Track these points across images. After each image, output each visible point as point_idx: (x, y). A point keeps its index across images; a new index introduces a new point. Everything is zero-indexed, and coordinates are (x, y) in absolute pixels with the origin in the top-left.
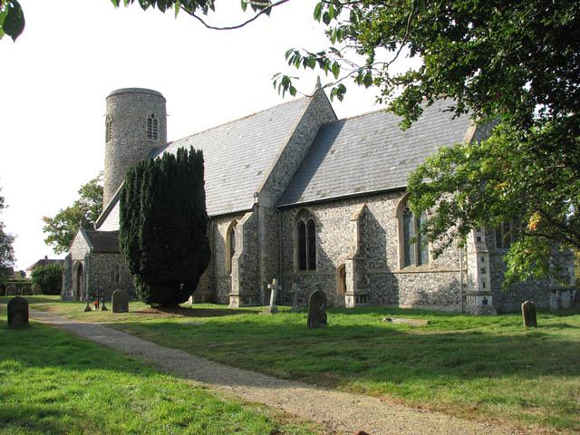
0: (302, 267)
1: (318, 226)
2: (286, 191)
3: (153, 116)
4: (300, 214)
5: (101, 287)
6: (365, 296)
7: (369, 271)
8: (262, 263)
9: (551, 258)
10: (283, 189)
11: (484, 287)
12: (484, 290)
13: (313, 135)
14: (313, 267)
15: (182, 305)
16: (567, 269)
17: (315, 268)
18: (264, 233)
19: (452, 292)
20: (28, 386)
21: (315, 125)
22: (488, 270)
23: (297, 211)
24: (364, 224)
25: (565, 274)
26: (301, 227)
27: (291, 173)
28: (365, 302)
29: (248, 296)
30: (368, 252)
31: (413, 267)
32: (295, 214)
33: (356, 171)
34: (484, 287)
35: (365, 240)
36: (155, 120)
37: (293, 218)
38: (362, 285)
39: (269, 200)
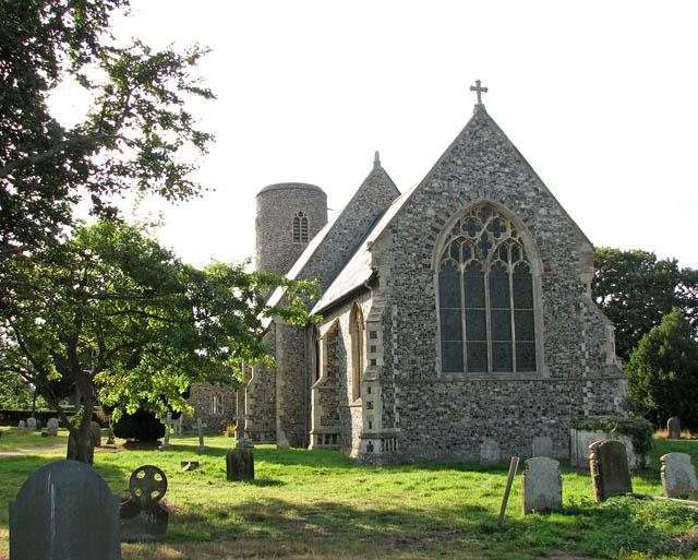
9: (589, 384)
11: (370, 427)
16: (612, 401)
18: (282, 356)
34: (370, 427)
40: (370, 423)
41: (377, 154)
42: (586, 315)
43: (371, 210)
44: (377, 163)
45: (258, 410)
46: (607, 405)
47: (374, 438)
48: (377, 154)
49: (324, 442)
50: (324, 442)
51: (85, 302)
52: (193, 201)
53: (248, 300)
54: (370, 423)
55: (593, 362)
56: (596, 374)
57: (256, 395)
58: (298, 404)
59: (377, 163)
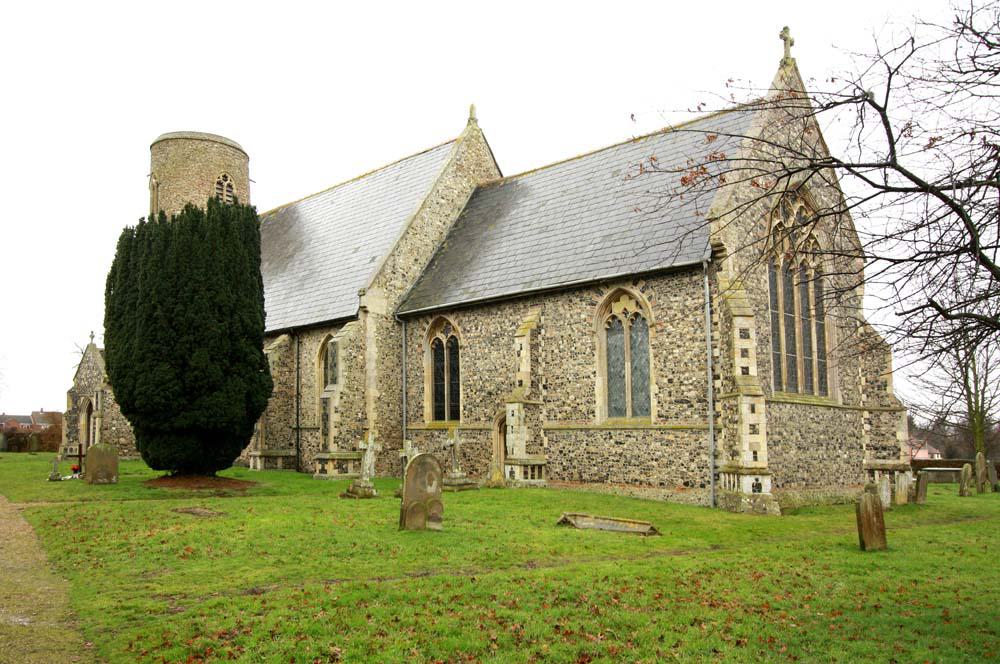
0: (439, 415)
1: (294, 213)
2: (413, 289)
3: (225, 178)
4: (435, 326)
5: (122, 440)
6: (540, 467)
7: (547, 424)
8: (371, 406)
9: (866, 414)
10: (409, 287)
11: (755, 458)
12: (759, 464)
13: (463, 202)
14: (455, 415)
15: (221, 474)
16: (894, 434)
17: (458, 418)
18: (375, 356)
19: (693, 466)
20: (565, 367)
21: (460, 190)
22: (763, 428)
23: (431, 321)
24: (538, 345)
25: (891, 443)
26: (438, 348)
27: (424, 261)
28: (540, 477)
29: (346, 460)
30: (544, 393)
31: (628, 420)
32: (427, 327)
33: (526, 256)
34: (755, 458)
35: (540, 372)
36: (229, 186)
37: (425, 334)
38: (534, 448)
39: (384, 303)
40: (755, 453)
41: (472, 109)
42: (862, 335)
43: (469, 181)
44: (472, 120)
45: (344, 429)
46: (888, 439)
47: (763, 475)
48: (472, 109)
49: (536, 477)
50: (529, 476)
51: (785, 230)
52: (476, 105)
53: (267, 263)
54: (755, 453)
55: (870, 390)
56: (874, 403)
57: (343, 410)
58: (394, 423)
59: (472, 120)
